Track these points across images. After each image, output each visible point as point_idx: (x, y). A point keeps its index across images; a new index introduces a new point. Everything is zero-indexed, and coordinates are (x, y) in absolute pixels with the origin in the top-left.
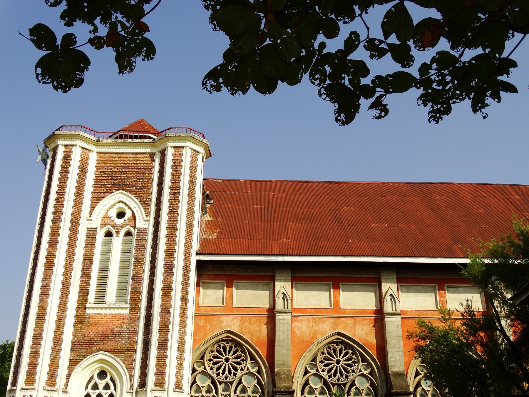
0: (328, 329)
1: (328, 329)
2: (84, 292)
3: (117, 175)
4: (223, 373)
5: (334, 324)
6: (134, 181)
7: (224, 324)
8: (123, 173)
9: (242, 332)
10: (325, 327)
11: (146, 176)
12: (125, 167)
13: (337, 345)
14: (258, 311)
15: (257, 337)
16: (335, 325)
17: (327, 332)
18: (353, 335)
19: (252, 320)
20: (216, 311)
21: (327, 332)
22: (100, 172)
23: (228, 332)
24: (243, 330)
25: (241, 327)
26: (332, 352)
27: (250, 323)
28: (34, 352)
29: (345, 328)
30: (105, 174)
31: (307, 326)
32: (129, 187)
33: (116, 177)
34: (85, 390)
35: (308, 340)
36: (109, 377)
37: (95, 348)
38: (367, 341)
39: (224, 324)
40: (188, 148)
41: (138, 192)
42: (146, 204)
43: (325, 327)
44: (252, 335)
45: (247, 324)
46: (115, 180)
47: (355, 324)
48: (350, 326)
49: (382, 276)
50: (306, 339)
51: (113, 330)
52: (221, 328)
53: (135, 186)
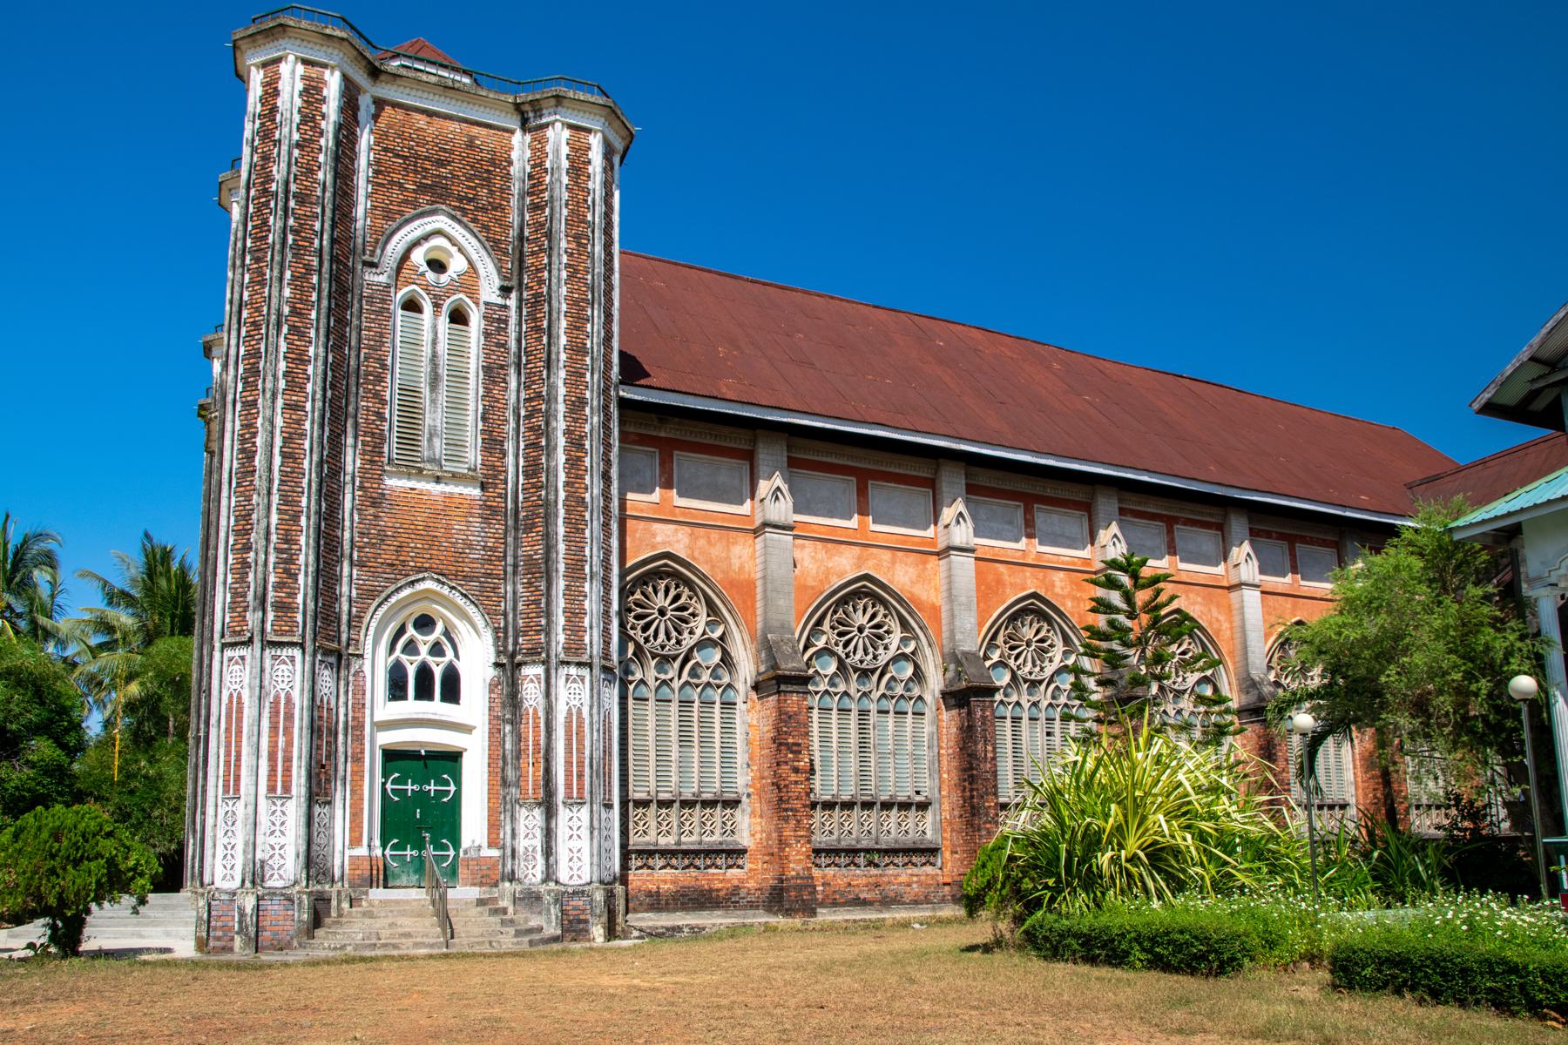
0: (848, 568)
1: (848, 568)
2: (373, 434)
3: (428, 165)
4: (669, 639)
5: (859, 558)
6: (469, 187)
7: (659, 539)
8: (441, 163)
9: (694, 559)
10: (844, 562)
11: (498, 182)
12: (445, 151)
13: (633, 594)
14: (723, 520)
15: (723, 572)
16: (860, 561)
17: (846, 572)
18: (889, 581)
19: (713, 536)
20: (642, 511)
21: (846, 572)
22: (386, 150)
23: (668, 555)
24: (696, 554)
25: (690, 548)
26: (639, 610)
27: (709, 542)
28: (286, 562)
29: (878, 567)
30: (398, 156)
31: (813, 557)
32: (460, 199)
33: (426, 170)
34: (390, 654)
35: (813, 584)
36: (440, 627)
37: (412, 564)
38: (912, 594)
39: (659, 539)
40: (558, 125)
41: (480, 216)
42: (500, 249)
43: (844, 562)
44: (713, 567)
45: (702, 542)
46: (425, 178)
47: (893, 562)
48: (885, 564)
49: (761, 456)
50: (811, 583)
51: (448, 528)
52: (653, 547)
53: (470, 200)
